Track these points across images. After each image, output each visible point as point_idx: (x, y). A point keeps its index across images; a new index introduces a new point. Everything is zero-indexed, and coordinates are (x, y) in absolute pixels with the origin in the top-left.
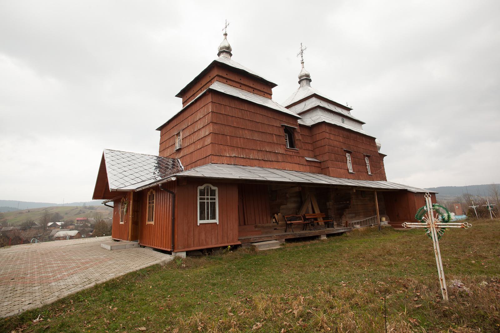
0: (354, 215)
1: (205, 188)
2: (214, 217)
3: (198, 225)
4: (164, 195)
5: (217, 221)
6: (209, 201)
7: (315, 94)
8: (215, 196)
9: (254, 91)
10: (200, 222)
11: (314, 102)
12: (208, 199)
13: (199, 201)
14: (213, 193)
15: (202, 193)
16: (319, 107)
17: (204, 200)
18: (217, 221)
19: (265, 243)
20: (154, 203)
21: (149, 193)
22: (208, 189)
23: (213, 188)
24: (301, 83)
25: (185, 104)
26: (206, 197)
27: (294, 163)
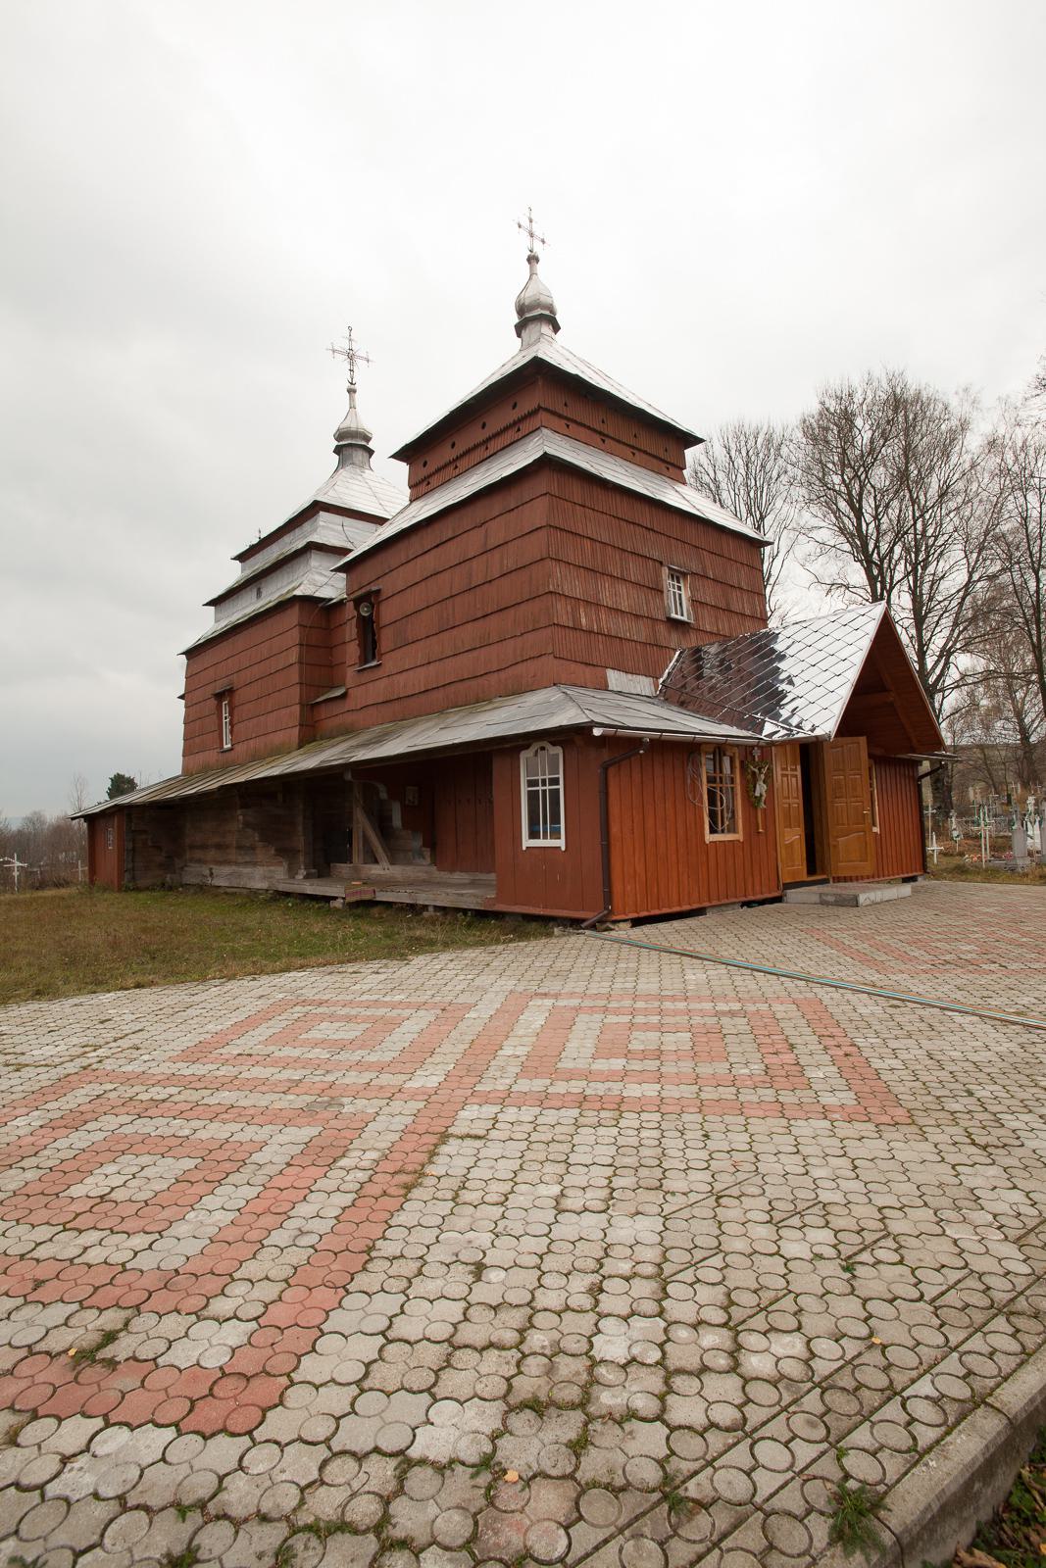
3: (524, 848)
4: (883, 774)
5: (561, 843)
9: (635, 454)
10: (709, 838)
13: (524, 790)
17: (534, 786)
18: (561, 843)
19: (565, 911)
20: (709, 791)
21: (824, 898)
24: (524, 334)
25: (423, 488)
27: (582, 663)
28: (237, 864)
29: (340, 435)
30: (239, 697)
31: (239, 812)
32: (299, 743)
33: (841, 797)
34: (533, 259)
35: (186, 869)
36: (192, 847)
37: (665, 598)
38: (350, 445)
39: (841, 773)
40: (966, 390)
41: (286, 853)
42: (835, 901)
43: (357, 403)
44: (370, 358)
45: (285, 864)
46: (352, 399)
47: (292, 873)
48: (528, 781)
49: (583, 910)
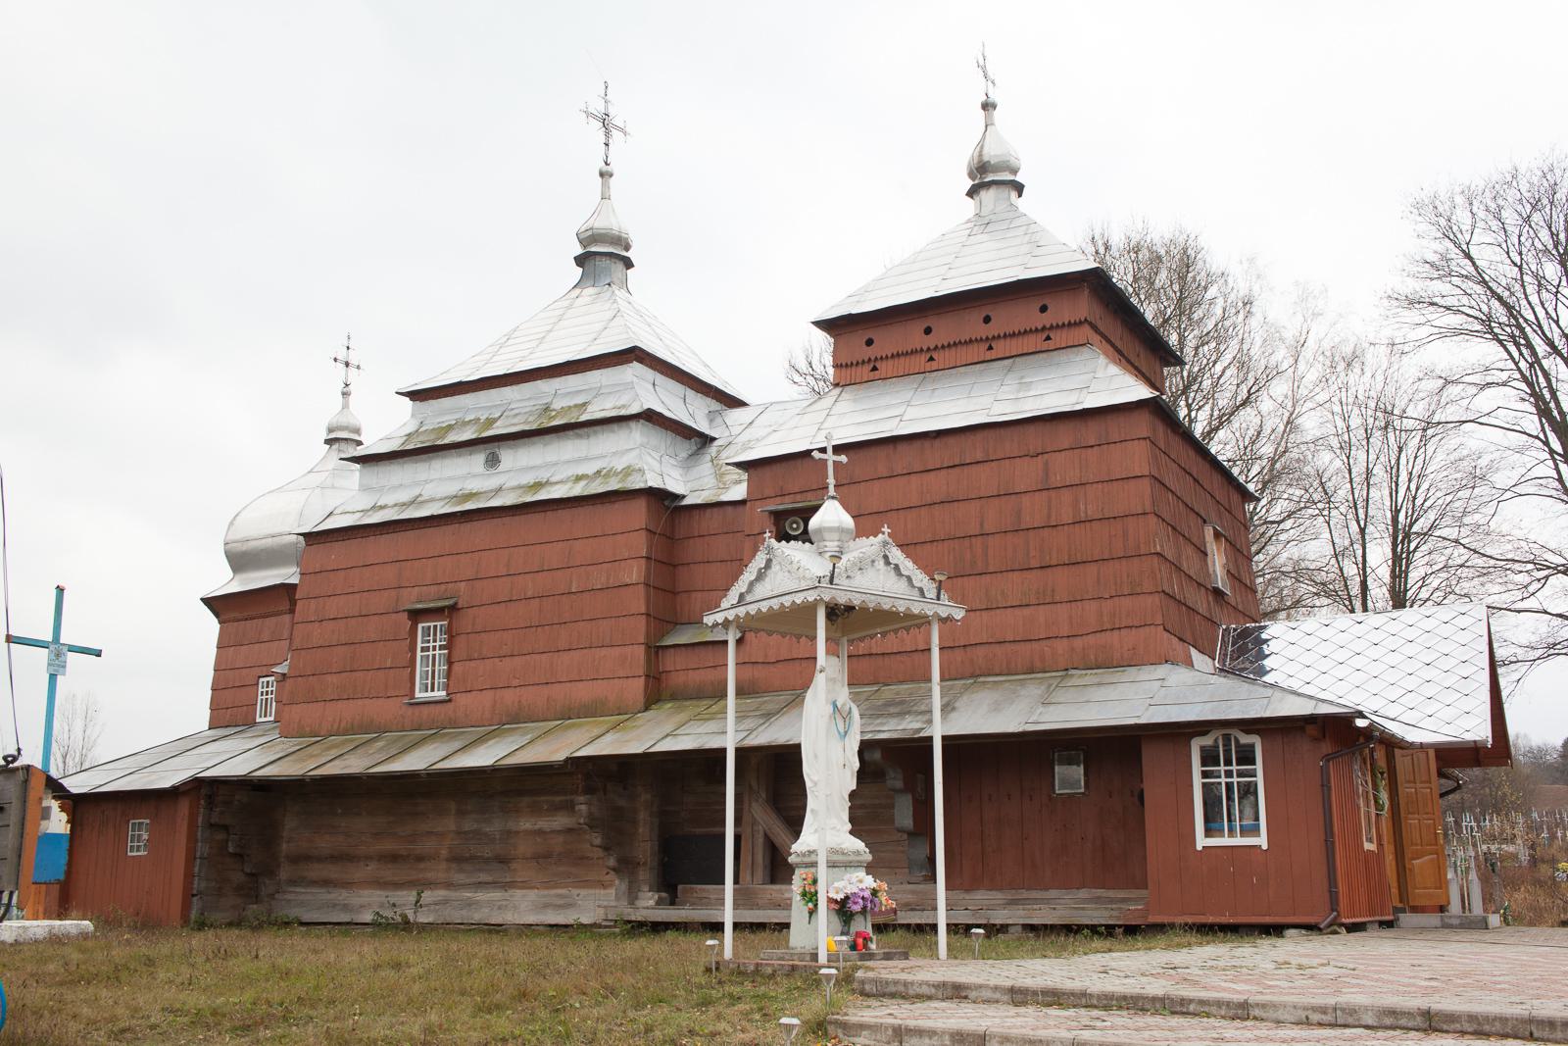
0: (717, 699)
1: (1216, 740)
2: (1254, 831)
5: (1262, 841)
6: (1235, 780)
7: (649, 410)
8: (1254, 764)
11: (641, 390)
12: (1229, 774)
14: (1246, 756)
15: (1209, 758)
16: (650, 417)
18: (1262, 841)
21: (1446, 920)
22: (1227, 744)
23: (1245, 739)
26: (1222, 768)
28: (449, 885)
29: (589, 238)
30: (465, 621)
31: (582, 799)
32: (645, 703)
33: (1414, 813)
34: (988, 106)
35: (277, 896)
36: (297, 859)
37: (1209, 562)
38: (611, 255)
39: (1412, 785)
40: (1251, 260)
41: (626, 867)
42: (1461, 924)
43: (613, 192)
44: (628, 130)
45: (627, 880)
46: (605, 187)
47: (632, 897)
48: (1203, 772)
49: (1294, 915)
